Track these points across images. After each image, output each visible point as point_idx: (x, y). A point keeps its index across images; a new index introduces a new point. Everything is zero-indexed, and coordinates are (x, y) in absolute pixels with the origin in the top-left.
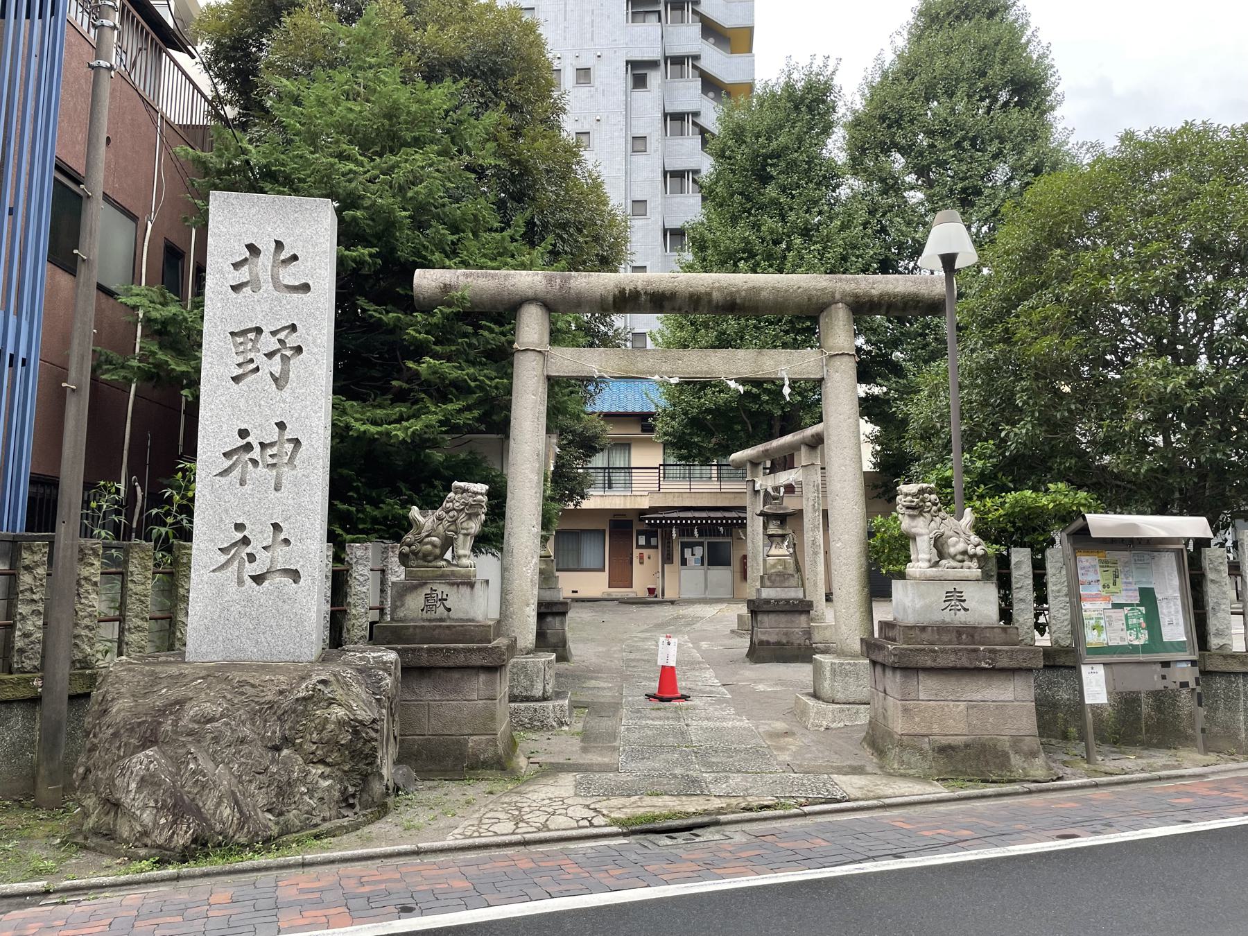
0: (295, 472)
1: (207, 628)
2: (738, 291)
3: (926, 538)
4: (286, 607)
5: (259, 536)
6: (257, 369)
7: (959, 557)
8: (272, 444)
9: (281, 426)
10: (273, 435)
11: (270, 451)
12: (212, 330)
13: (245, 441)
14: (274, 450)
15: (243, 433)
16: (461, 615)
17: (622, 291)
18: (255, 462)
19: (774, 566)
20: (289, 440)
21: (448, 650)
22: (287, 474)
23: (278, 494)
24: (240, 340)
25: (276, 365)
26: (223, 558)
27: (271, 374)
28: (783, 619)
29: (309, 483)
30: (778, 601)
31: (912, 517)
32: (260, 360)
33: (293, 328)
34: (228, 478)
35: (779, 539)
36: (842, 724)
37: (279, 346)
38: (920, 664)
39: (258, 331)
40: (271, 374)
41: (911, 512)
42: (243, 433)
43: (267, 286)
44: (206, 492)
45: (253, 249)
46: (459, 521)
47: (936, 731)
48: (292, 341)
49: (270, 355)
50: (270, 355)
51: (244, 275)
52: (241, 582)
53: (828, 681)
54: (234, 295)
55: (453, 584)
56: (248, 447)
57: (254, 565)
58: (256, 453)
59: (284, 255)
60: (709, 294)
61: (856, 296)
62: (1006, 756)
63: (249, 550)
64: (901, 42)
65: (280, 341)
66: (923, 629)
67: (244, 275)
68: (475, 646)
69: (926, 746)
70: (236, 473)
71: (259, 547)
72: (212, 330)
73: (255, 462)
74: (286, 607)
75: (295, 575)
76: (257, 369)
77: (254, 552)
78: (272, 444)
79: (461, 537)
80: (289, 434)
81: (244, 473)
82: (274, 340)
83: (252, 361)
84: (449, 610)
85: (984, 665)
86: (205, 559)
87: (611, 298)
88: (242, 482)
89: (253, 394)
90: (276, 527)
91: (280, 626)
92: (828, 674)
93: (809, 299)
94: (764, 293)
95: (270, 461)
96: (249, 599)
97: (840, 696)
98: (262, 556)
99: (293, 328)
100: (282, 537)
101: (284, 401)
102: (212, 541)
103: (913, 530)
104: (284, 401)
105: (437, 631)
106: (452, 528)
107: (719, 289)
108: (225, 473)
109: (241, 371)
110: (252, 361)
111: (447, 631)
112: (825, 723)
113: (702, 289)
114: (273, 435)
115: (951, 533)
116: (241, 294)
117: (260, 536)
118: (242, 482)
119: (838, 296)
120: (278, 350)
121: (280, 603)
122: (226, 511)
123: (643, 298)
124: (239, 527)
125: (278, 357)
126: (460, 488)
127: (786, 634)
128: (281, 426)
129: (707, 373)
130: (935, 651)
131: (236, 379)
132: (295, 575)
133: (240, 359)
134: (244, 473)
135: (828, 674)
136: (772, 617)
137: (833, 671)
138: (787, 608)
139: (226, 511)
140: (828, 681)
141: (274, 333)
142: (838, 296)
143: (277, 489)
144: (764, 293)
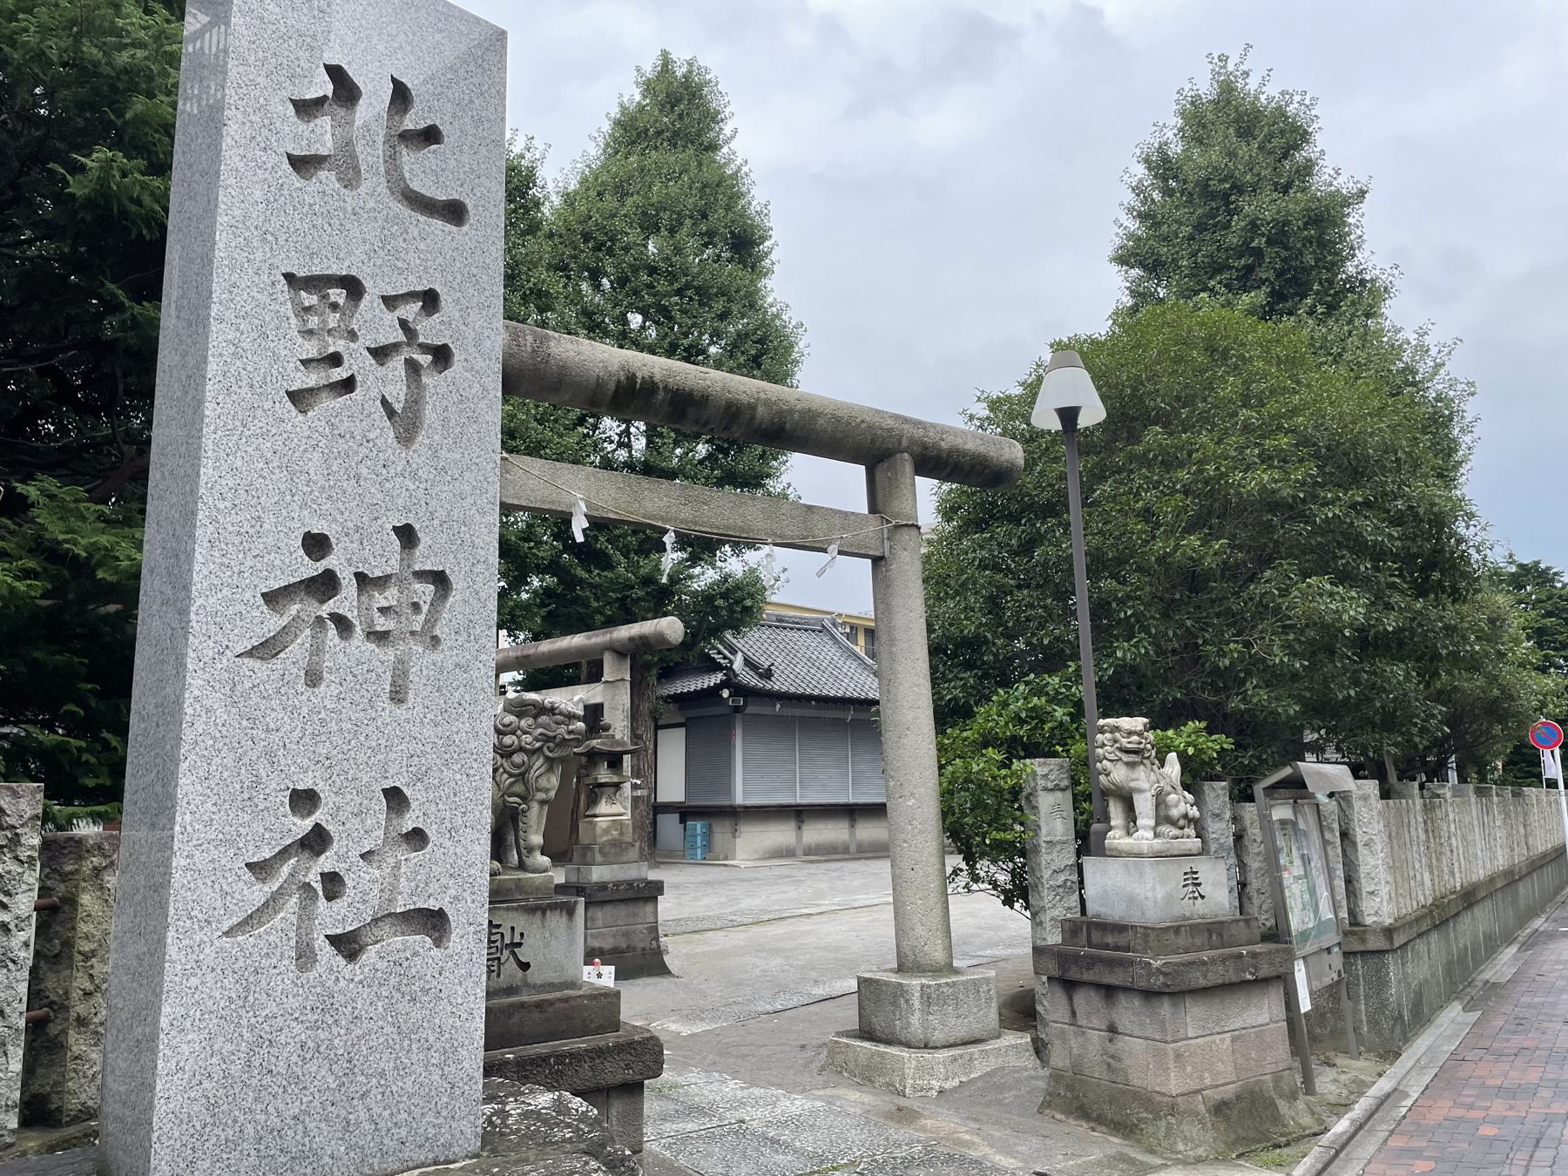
0: (437, 656)
1: (212, 1107)
2: (791, 411)
3: (1148, 795)
4: (417, 1014)
5: (354, 823)
6: (348, 385)
7: (1182, 822)
8: (382, 582)
9: (407, 535)
10: (385, 558)
11: (380, 600)
12: (241, 256)
13: (321, 566)
14: (389, 597)
15: (316, 545)
16: (551, 976)
17: (631, 378)
18: (343, 624)
19: (606, 831)
20: (421, 575)
21: (560, 1057)
22: (422, 661)
23: (400, 712)
24: (309, 299)
25: (392, 380)
26: (258, 893)
27: (384, 402)
28: (622, 911)
29: (469, 685)
30: (617, 884)
31: (1131, 765)
32: (357, 362)
33: (430, 300)
34: (276, 664)
35: (612, 790)
36: (956, 1083)
37: (400, 336)
38: (1193, 985)
39: (353, 287)
40: (384, 402)
41: (1126, 758)
42: (316, 545)
43: (374, 184)
44: (215, 700)
45: (345, 89)
46: (533, 774)
47: (1208, 1082)
48: (431, 330)
49: (381, 354)
50: (381, 354)
51: (321, 135)
52: (305, 957)
53: (917, 1014)
54: (295, 180)
55: (532, 910)
56: (326, 585)
57: (340, 905)
58: (346, 601)
59: (411, 122)
60: (753, 408)
61: (925, 447)
62: (1272, 1105)
63: (326, 862)
64: (594, 151)
65: (403, 324)
66: (1177, 930)
67: (321, 135)
68: (580, 1044)
69: (1202, 1108)
70: (297, 651)
71: (354, 855)
72: (241, 256)
73: (343, 624)
74: (417, 1014)
75: (433, 922)
76: (348, 385)
77: (340, 868)
78: (382, 582)
79: (535, 806)
80: (424, 560)
81: (317, 650)
82: (391, 318)
83: (335, 360)
84: (525, 966)
85: (1249, 977)
86: (210, 896)
87: (612, 386)
88: (313, 678)
89: (342, 445)
90: (395, 798)
91: (402, 1070)
92: (917, 1004)
93: (873, 441)
94: (821, 421)
95: (381, 624)
96: (326, 1005)
97: (938, 1036)
98: (359, 879)
99: (430, 300)
100: (408, 824)
101: (414, 475)
102: (230, 842)
103: (1132, 784)
104: (414, 475)
105: (516, 1019)
106: (519, 788)
107: (767, 403)
108: (267, 649)
109: (312, 379)
110: (335, 360)
111: (536, 1016)
112: (936, 1084)
113: (744, 399)
114: (385, 558)
115: (1169, 789)
116: (312, 186)
117: (355, 825)
118: (313, 678)
119: (905, 443)
120: (395, 347)
121: (404, 1006)
122: (270, 755)
123: (661, 395)
124: (304, 800)
125: (397, 364)
126: (534, 704)
127: (626, 935)
128: (407, 535)
129: (742, 529)
130: (1204, 963)
131: (299, 398)
132: (433, 922)
133: (311, 349)
134: (317, 650)
135: (917, 1004)
136: (608, 909)
137: (927, 999)
138: (630, 894)
139: (270, 755)
140: (917, 1014)
141: (390, 302)
142: (905, 443)
143: (398, 696)
144: (821, 421)
